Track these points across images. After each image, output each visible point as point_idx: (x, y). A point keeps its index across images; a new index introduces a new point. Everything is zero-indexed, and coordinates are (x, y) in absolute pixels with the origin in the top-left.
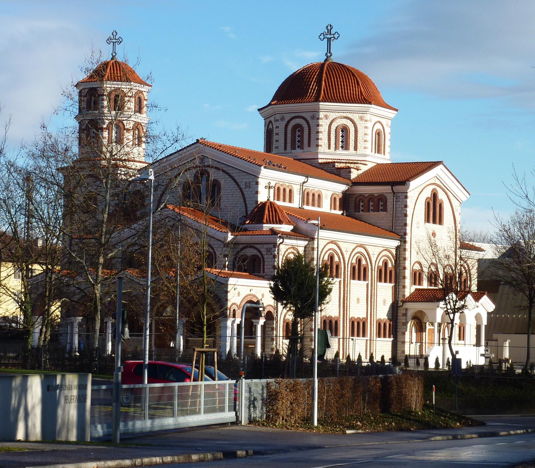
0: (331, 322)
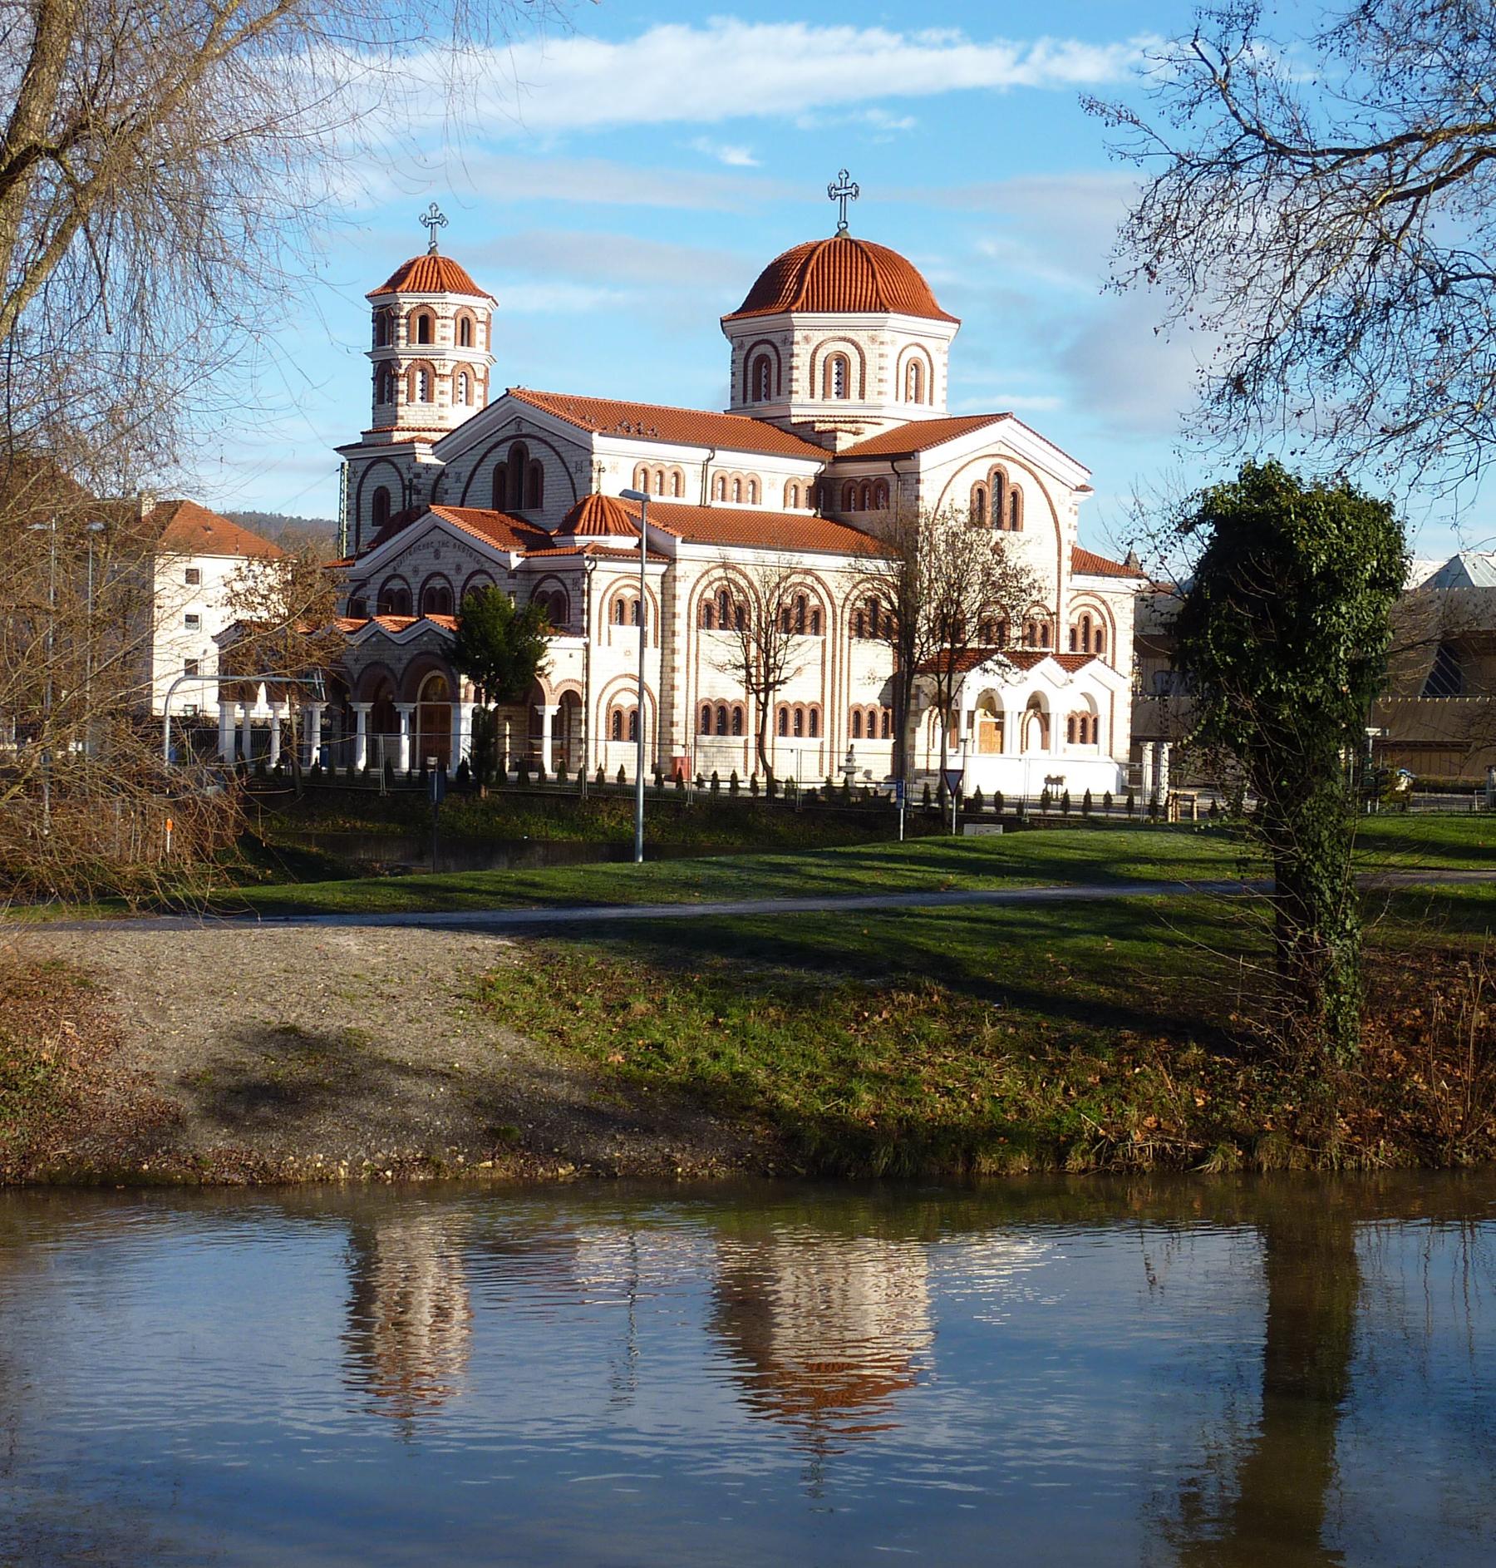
0: (722, 709)
